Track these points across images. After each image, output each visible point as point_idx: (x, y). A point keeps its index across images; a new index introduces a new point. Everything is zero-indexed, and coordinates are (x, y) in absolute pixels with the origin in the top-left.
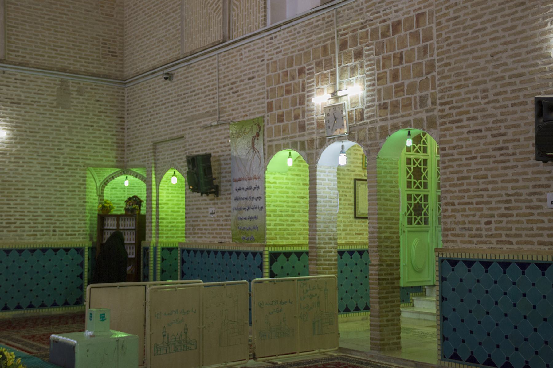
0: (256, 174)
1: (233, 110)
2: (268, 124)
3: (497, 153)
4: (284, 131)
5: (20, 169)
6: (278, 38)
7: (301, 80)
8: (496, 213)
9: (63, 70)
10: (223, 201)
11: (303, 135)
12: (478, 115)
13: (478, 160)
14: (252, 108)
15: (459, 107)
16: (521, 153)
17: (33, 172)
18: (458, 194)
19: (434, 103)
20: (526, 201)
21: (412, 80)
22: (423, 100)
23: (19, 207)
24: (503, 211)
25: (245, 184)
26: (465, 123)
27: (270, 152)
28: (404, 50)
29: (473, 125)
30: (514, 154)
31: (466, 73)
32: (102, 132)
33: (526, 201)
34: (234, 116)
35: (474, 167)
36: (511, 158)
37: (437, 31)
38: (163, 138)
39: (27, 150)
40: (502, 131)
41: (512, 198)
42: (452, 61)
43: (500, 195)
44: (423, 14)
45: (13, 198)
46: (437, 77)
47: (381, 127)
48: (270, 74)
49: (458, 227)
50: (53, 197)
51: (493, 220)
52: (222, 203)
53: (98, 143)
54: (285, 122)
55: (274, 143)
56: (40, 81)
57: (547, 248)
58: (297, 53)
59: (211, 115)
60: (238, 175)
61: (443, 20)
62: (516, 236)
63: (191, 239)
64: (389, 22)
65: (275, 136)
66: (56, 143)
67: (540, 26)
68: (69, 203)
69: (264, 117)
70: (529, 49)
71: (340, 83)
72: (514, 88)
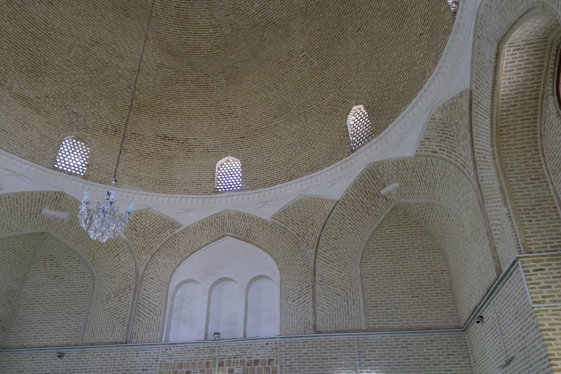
44: (273, 360)
48: (162, 370)
58: (186, 362)
61: (284, 365)
64: (253, 359)
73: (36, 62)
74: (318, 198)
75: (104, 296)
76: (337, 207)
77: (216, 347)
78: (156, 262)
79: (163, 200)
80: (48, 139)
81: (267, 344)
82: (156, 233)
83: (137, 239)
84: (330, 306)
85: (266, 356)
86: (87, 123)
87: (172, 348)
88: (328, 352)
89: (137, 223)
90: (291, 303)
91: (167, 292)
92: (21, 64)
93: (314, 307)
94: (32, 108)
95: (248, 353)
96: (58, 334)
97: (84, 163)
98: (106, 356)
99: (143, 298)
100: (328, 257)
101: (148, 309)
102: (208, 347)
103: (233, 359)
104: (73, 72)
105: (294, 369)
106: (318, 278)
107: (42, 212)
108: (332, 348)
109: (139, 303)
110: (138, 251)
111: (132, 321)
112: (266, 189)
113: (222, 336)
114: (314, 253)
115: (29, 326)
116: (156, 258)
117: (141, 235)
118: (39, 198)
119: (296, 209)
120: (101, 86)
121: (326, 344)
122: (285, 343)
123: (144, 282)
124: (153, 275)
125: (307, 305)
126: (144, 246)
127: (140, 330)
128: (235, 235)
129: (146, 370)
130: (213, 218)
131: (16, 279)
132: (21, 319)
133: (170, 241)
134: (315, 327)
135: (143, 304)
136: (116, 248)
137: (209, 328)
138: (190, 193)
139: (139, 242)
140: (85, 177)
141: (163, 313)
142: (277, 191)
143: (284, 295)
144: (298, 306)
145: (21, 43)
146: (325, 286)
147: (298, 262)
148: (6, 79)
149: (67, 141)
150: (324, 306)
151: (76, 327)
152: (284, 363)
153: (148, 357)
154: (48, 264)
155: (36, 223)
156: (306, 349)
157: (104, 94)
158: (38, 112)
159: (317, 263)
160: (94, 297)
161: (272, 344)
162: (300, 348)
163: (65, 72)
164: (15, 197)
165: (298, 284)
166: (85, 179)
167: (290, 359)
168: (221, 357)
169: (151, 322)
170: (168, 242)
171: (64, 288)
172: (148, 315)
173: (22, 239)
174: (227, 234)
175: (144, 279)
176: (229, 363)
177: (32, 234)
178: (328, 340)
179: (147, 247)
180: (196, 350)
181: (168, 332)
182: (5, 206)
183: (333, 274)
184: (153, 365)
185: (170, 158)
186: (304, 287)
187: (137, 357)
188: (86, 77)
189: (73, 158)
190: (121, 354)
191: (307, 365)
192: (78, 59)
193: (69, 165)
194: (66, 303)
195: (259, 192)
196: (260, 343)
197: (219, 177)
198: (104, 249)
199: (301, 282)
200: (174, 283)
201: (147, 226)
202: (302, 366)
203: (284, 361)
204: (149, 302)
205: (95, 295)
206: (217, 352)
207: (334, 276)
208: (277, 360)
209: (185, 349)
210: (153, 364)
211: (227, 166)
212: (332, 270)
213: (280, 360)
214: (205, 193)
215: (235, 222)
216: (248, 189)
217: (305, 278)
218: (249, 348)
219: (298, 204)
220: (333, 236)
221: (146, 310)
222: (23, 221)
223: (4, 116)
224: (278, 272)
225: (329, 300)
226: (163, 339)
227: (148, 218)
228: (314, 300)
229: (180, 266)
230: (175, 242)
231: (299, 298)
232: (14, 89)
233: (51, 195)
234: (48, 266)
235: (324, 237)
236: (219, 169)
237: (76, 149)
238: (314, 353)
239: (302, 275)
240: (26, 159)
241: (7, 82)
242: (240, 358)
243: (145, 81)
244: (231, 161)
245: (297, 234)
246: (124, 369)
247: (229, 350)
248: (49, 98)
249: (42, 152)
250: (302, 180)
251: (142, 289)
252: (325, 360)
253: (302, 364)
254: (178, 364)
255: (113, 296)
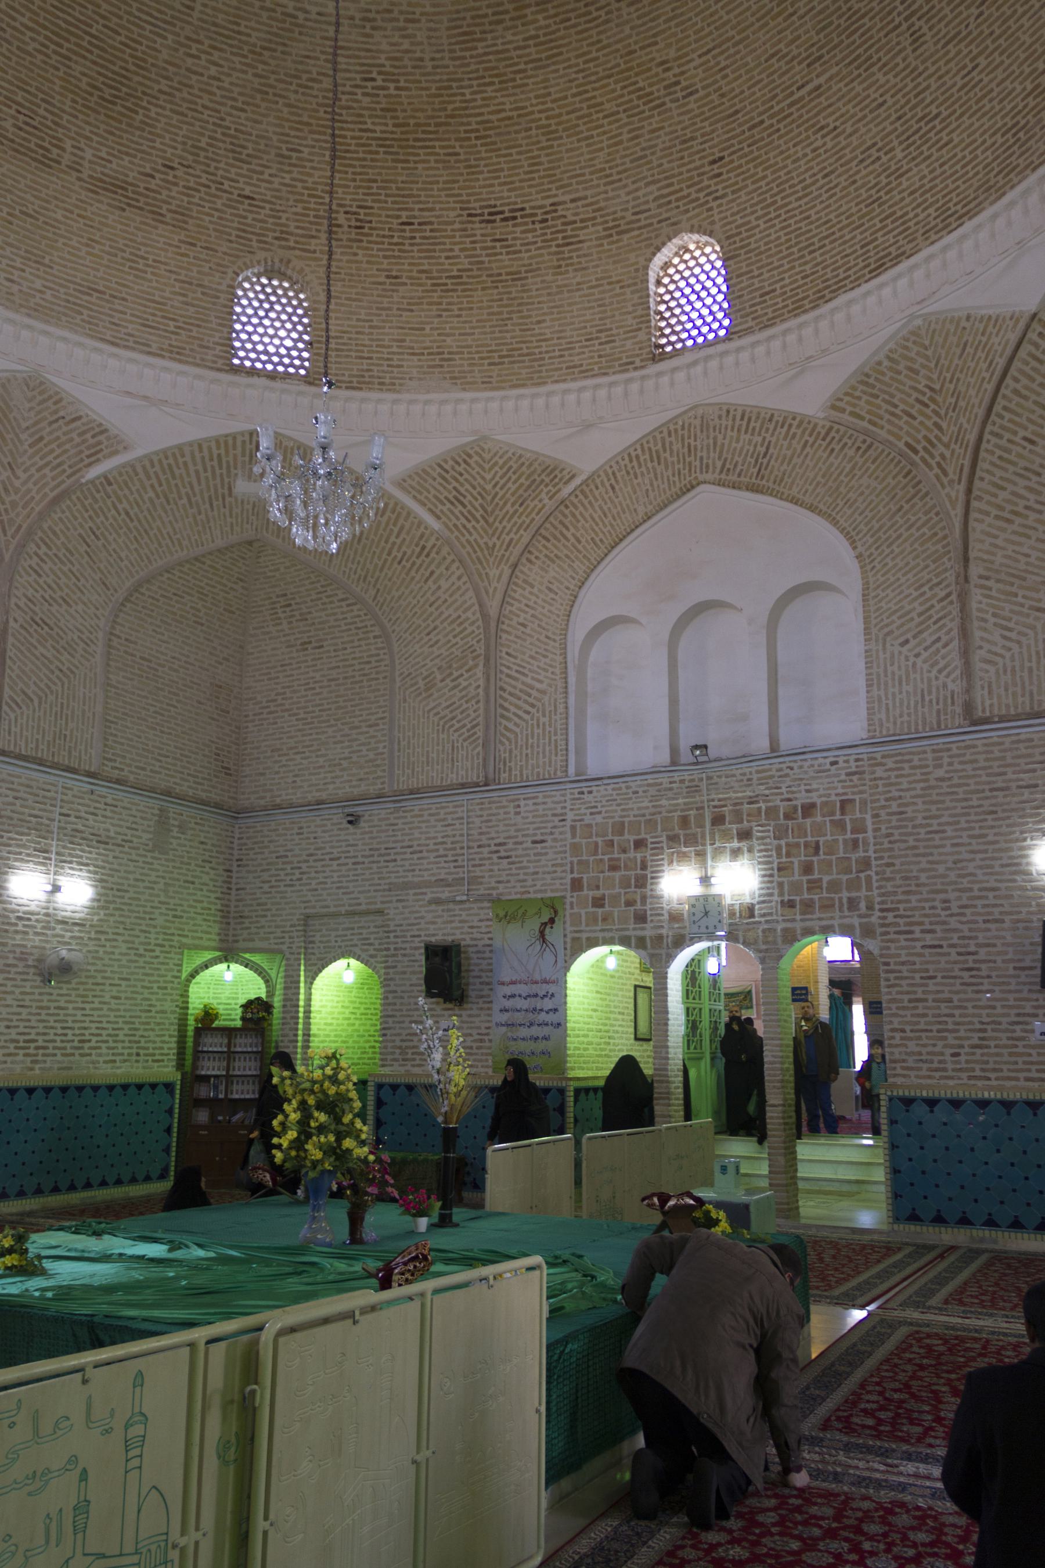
0: (547, 975)
1: (499, 882)
2: (572, 908)
3: (966, 974)
4: (604, 920)
5: (101, 950)
6: (595, 794)
7: (639, 856)
8: (966, 1043)
9: (168, 793)
10: (474, 1012)
11: (643, 929)
12: (938, 928)
13: (939, 980)
14: (539, 883)
15: (908, 917)
16: (998, 976)
17: (117, 957)
18: (909, 1019)
19: (870, 907)
20: (1006, 1030)
21: (834, 876)
22: (853, 904)
23: (96, 1013)
24: (976, 1041)
25: (522, 989)
26: (918, 935)
27: (578, 948)
28: (822, 840)
29: (929, 940)
30: (989, 977)
31: (917, 878)
32: (205, 893)
33: (1006, 1030)
34: (501, 890)
35: (932, 988)
36: (986, 981)
37: (873, 823)
38: (332, 909)
39: (112, 919)
40: (972, 949)
41: (989, 1027)
42: (897, 862)
43: (970, 1023)
44: (852, 801)
45: (90, 999)
46: (875, 878)
47: (785, 930)
48: (577, 840)
49: (911, 1059)
50: (140, 997)
51: (962, 1051)
52: (470, 1016)
53: (199, 910)
54: (607, 908)
55: (584, 936)
56: (134, 807)
57: (1036, 1085)
58: (632, 818)
59: (449, 885)
60: (506, 975)
61: (882, 813)
62: (994, 1070)
63: (386, 1071)
64: (799, 803)
65: (587, 925)
66: (148, 909)
67: (1017, 840)
68: (158, 1008)
69: (564, 897)
70: (1004, 862)
71: (713, 867)
72: (986, 902)
73: (116, 69)
74: (968, 318)
75: (419, 679)
76: (1032, 335)
77: (701, 780)
78: (525, 581)
79: (516, 409)
80: (200, 290)
81: (833, 763)
82: (513, 505)
83: (469, 526)
84: (1016, 648)
85: (833, 792)
86: (283, 221)
87: (594, 789)
88: (1009, 770)
89: (462, 485)
90: (897, 649)
91: (564, 655)
92: (84, 86)
93: (966, 654)
94: (141, 209)
95: (784, 790)
96: (338, 773)
97: (300, 339)
98: (449, 817)
99: (508, 676)
100: (1008, 501)
101: (526, 702)
102: (682, 781)
103: (746, 806)
104: (213, 70)
105: (912, 819)
106: (975, 570)
107: (235, 491)
108: (1021, 761)
109: (502, 689)
110: (478, 559)
111: (492, 732)
112: (804, 318)
113: (713, 752)
114: (962, 497)
115: (276, 762)
116: (525, 570)
117: (478, 515)
118: (219, 455)
119: (901, 367)
120: (292, 96)
121: (1005, 751)
122: (883, 757)
123: (504, 636)
124: (522, 615)
125: (943, 651)
126: (491, 544)
127: (514, 752)
128: (723, 476)
129: (543, 841)
130: (659, 436)
131: (224, 659)
132: (258, 748)
133: (551, 519)
134: (968, 708)
135: (512, 690)
136: (423, 557)
137: (681, 735)
138: (586, 373)
139: (475, 535)
140: (309, 380)
141: (561, 708)
142: (839, 316)
143: (874, 631)
144: (917, 655)
145: (66, 21)
146: (999, 591)
147: (913, 530)
148: (60, 140)
149: (247, 285)
150: (994, 649)
151: (371, 755)
152: (884, 807)
153: (541, 813)
154: (282, 616)
155: (229, 520)
156: (946, 768)
157: (305, 119)
158: (158, 217)
159: (972, 524)
160: (398, 684)
161: (847, 761)
162: (927, 766)
163: (194, 77)
164: (165, 462)
165: (915, 594)
166: (310, 384)
167: (900, 797)
168: (716, 803)
169: (536, 731)
170: (547, 525)
171: (330, 669)
172: (526, 717)
173: (208, 562)
174: (701, 478)
175: (504, 627)
176: (738, 817)
177: (226, 548)
178: (1008, 740)
179: (498, 544)
180: (652, 791)
181: (581, 752)
182: (149, 489)
183: (1025, 550)
184: (557, 831)
185: (516, 277)
186: (934, 602)
187: (518, 813)
188: (249, 77)
189: (271, 331)
190: (481, 809)
191: (948, 809)
192: (215, 25)
193: (266, 352)
194: (342, 704)
195: (785, 333)
196: (816, 763)
197: (662, 308)
198: (395, 565)
199: (926, 588)
200: (578, 633)
201: (489, 487)
202: (934, 812)
203: (883, 803)
204: (523, 683)
205: (398, 679)
206: (705, 792)
207: (1027, 556)
208: (863, 803)
209: (624, 791)
210: (554, 827)
211: (681, 267)
212: (1022, 540)
213: (873, 801)
214: (627, 366)
215: (720, 437)
216: (749, 331)
217: (936, 576)
218: (787, 775)
219: (906, 348)
220: (1022, 433)
221: (520, 703)
222: (198, 518)
223: (85, 249)
224: (853, 565)
225: (1010, 630)
226: (572, 770)
227: (487, 466)
228: (965, 633)
229: (587, 584)
230: (566, 522)
231: (920, 632)
232: (86, 164)
233: (244, 442)
234: (285, 622)
235: (994, 440)
236: (659, 283)
237: (272, 303)
238: (968, 777)
239: (927, 566)
240: (163, 357)
241: (63, 150)
242: (764, 801)
243: (406, 45)
244: (692, 247)
245: (907, 444)
246: (492, 842)
247: (736, 785)
248: (172, 168)
249: (195, 329)
250: (915, 266)
251: (503, 655)
252: (1000, 794)
253: (934, 807)
254: (614, 825)
255: (439, 677)
